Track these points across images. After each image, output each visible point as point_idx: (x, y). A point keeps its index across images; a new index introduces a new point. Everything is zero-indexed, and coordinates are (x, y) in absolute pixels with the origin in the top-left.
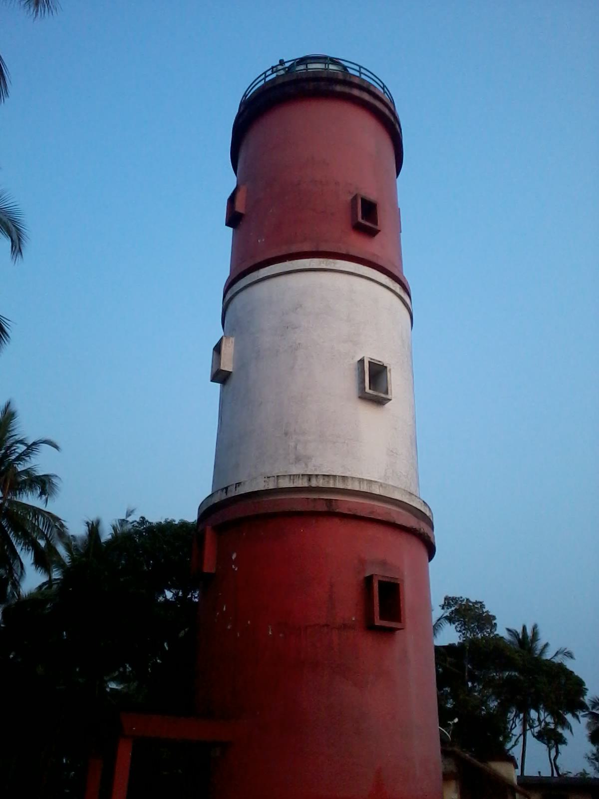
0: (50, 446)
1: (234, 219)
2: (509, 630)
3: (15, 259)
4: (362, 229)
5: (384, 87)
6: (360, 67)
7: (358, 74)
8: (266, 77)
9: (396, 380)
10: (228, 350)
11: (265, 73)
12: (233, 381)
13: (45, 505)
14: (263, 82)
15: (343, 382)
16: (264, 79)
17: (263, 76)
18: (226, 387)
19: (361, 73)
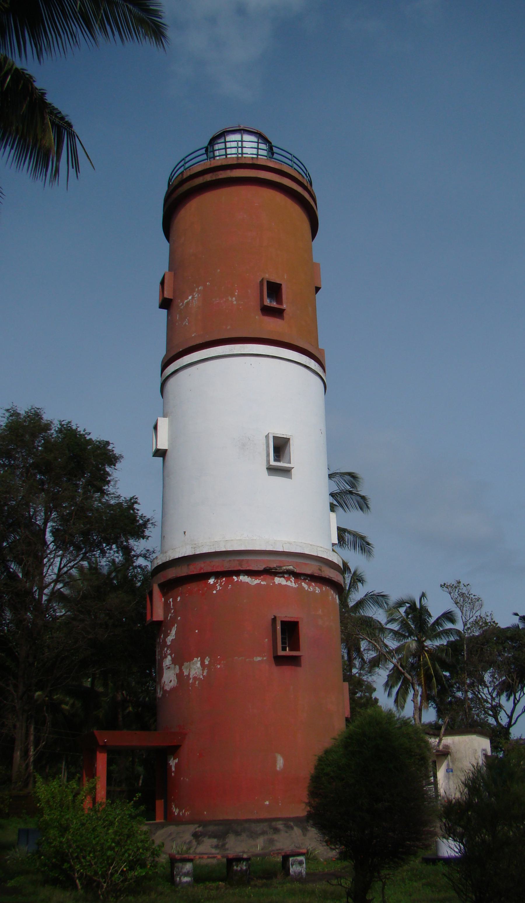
12: (168, 453)
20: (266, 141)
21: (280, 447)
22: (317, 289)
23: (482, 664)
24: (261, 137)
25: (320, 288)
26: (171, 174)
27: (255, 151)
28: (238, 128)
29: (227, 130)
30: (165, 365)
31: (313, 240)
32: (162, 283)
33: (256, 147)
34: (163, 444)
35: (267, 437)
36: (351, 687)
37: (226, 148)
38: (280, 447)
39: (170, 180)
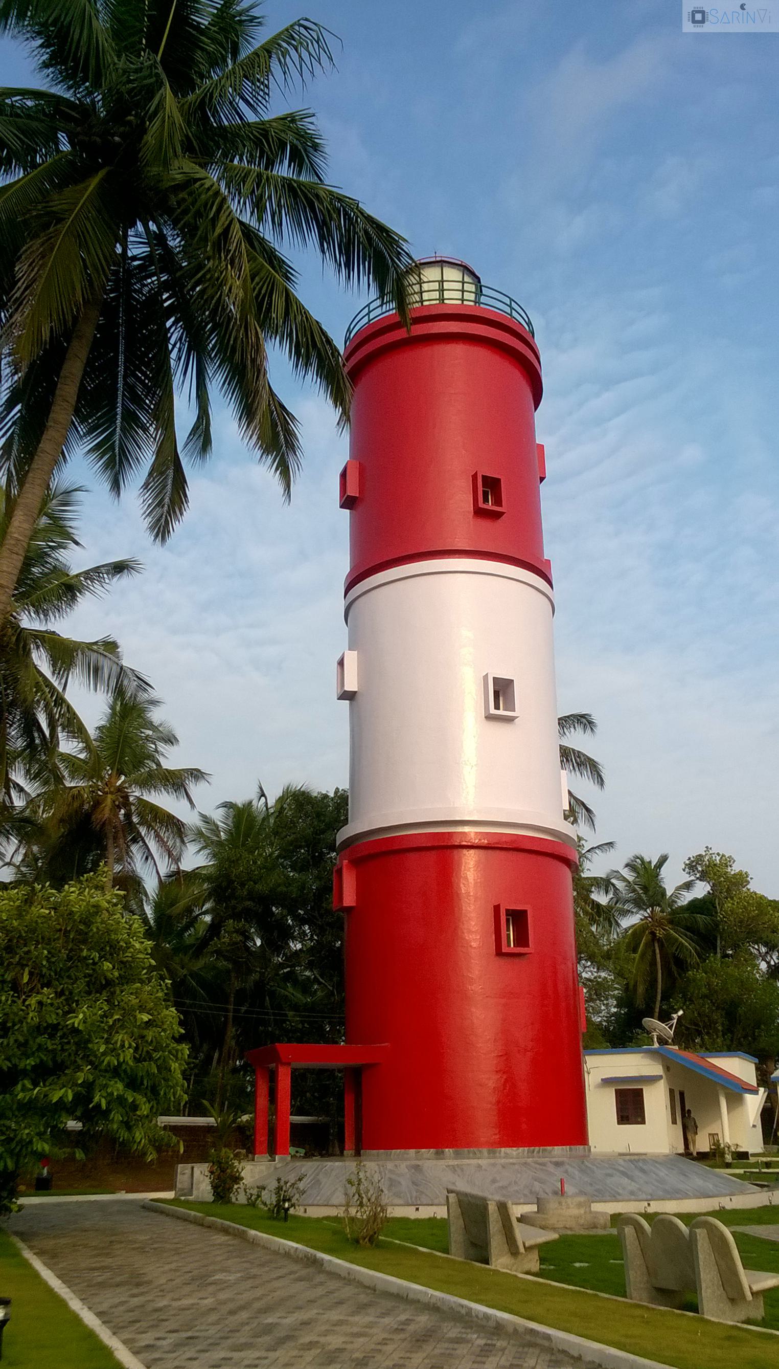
0: (667, 1367)
1: (348, 502)
2: (116, 486)
3: (561, 987)
4: (504, 518)
5: (529, 324)
6: (511, 300)
7: (508, 310)
8: (370, 312)
9: (519, 692)
10: (352, 659)
11: (368, 305)
12: (358, 696)
13: (185, 802)
14: (366, 320)
15: (471, 699)
16: (368, 314)
17: (366, 310)
18: (354, 702)
19: (512, 308)
20: (472, 274)
21: (502, 690)
22: (542, 479)
23: (294, 1059)
24: (466, 269)
25: (544, 478)
26: (336, 260)
27: (458, 295)
28: (433, 259)
29: (422, 261)
30: (350, 585)
31: (536, 409)
32: (344, 475)
33: (460, 297)
34: (351, 685)
35: (486, 677)
36: (78, 1113)
37: (421, 293)
38: (502, 690)
39: (349, 331)
